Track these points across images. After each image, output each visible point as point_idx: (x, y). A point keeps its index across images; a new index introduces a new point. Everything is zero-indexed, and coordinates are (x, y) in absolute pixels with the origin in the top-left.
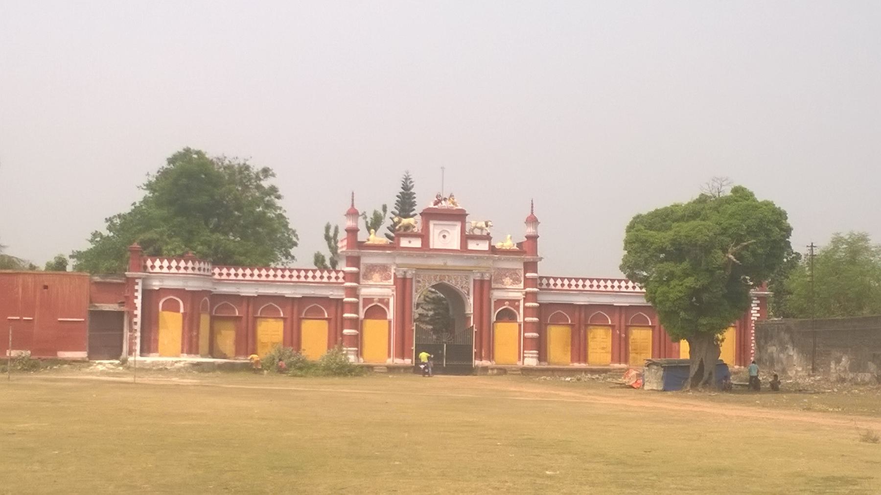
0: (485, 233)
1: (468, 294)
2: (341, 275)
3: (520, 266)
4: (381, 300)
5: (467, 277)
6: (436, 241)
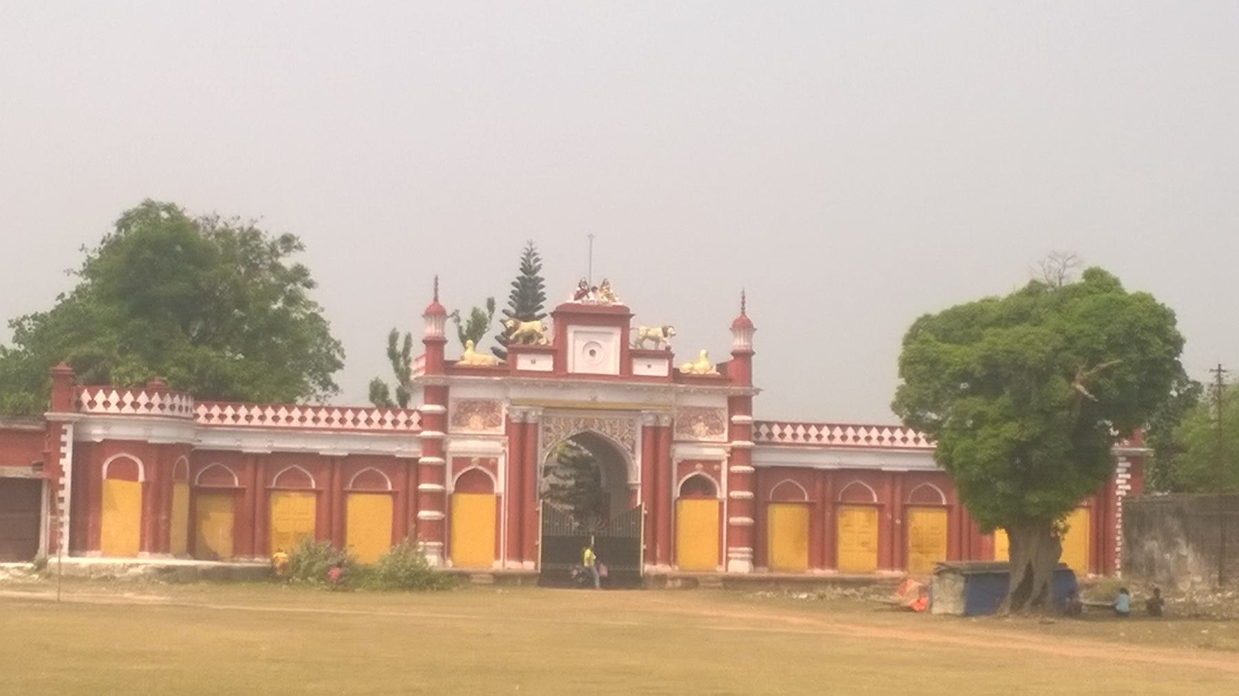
0: (662, 347)
1: (633, 451)
2: (415, 418)
3: (722, 403)
4: (484, 462)
5: (631, 423)
6: (578, 362)
